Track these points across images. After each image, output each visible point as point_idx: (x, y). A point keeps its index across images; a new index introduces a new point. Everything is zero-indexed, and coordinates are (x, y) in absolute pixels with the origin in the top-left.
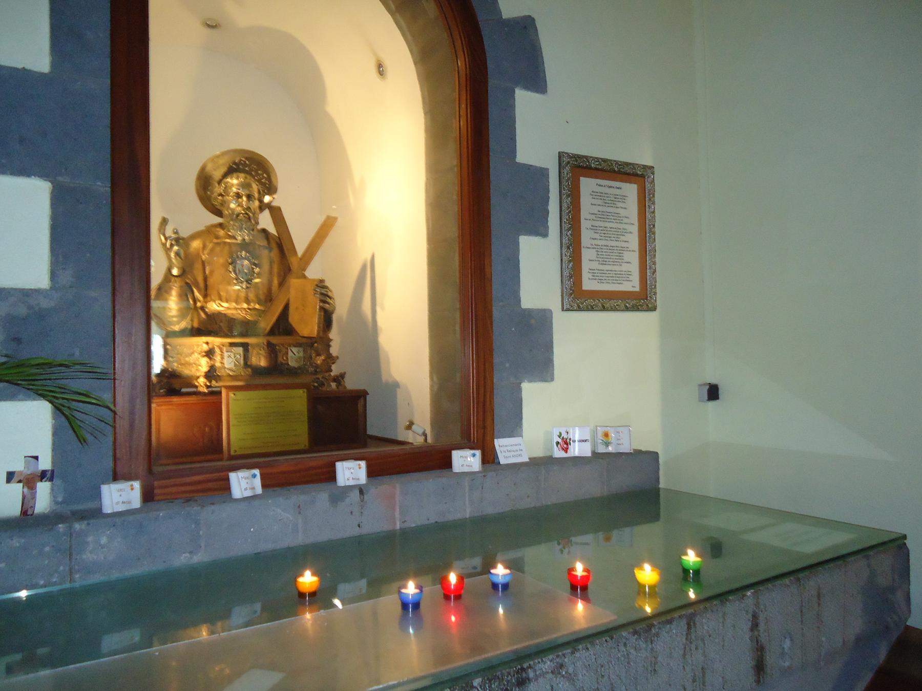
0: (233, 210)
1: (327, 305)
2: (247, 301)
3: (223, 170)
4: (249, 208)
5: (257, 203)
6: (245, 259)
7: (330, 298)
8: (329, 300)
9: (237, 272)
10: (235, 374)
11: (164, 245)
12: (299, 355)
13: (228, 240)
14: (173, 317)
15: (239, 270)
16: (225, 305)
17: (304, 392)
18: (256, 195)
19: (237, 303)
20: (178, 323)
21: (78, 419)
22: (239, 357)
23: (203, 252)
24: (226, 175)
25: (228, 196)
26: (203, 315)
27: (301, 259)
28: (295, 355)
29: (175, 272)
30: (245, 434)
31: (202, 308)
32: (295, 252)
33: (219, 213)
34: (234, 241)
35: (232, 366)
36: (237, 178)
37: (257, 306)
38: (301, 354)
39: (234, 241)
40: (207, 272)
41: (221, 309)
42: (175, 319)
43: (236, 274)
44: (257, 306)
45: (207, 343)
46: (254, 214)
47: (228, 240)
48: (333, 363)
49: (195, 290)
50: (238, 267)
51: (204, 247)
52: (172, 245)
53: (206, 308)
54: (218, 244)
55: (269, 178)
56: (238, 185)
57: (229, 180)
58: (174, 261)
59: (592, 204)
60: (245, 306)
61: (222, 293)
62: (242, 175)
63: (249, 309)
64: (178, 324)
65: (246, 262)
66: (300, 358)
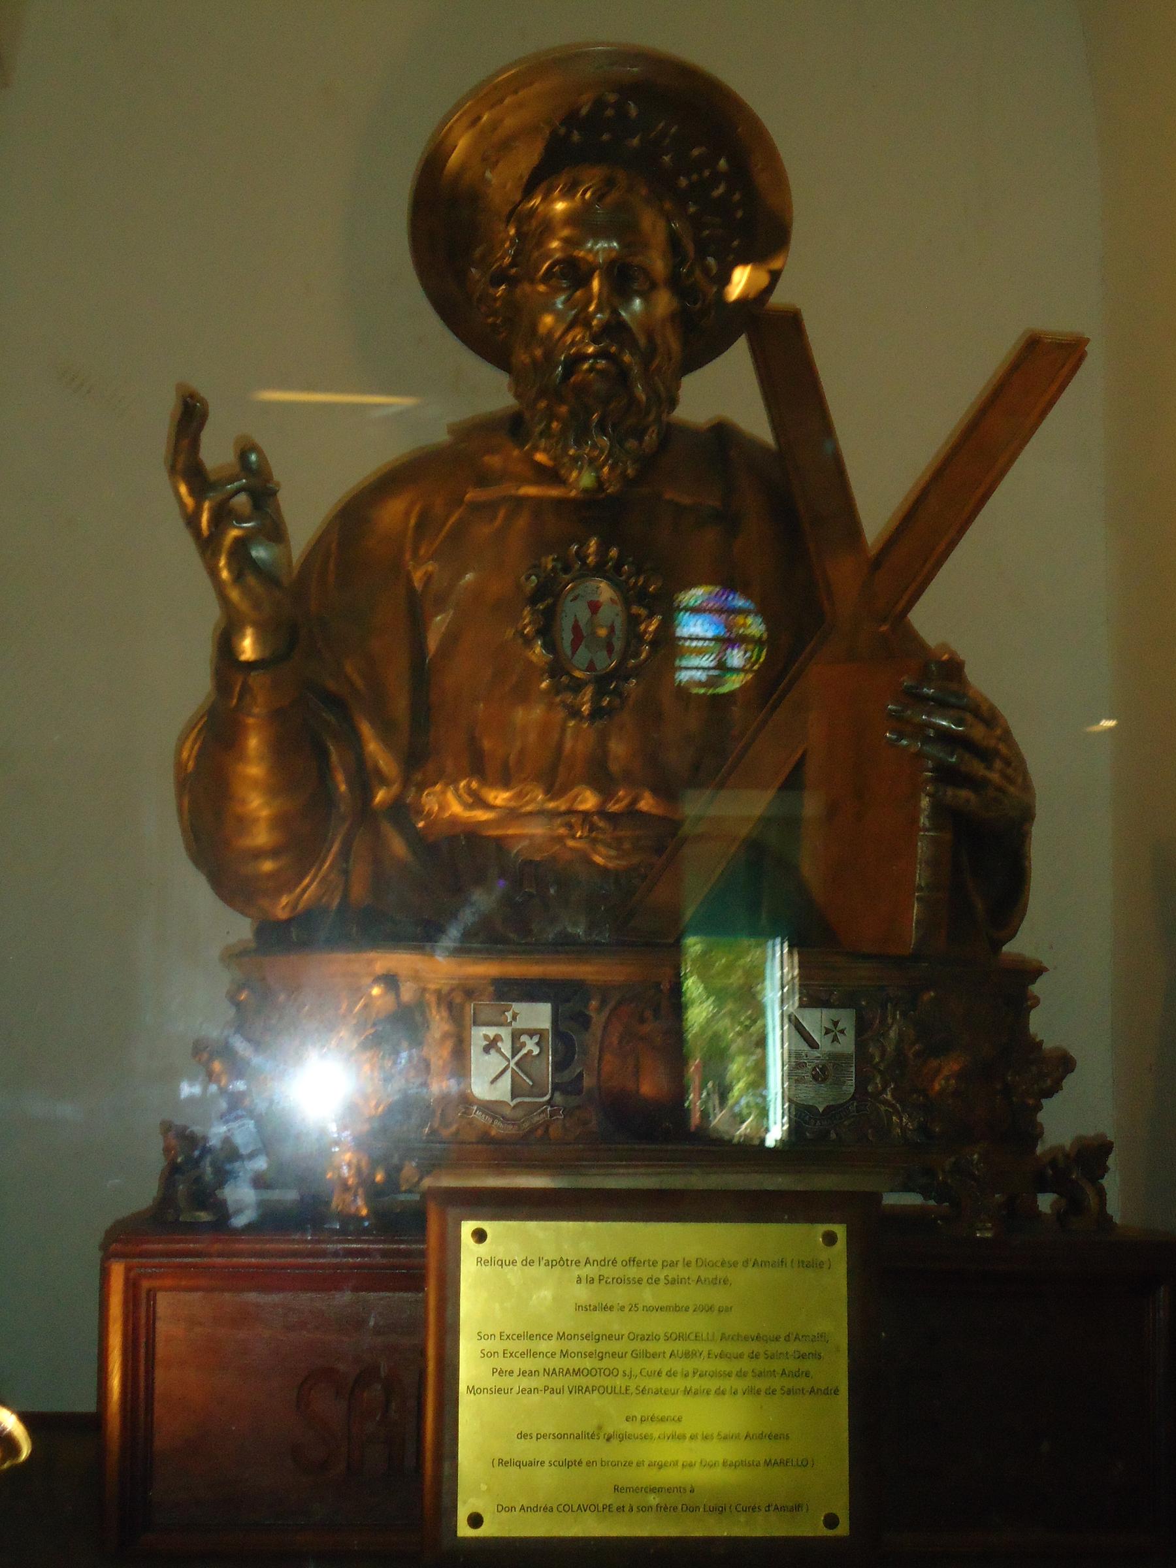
0: (549, 344)
1: (964, 794)
2: (602, 780)
3: (526, 158)
4: (615, 330)
5: (664, 302)
6: (599, 570)
7: (985, 755)
8: (978, 768)
9: (567, 637)
10: (510, 1130)
11: (192, 521)
12: (838, 1048)
13: (531, 490)
14: (258, 854)
15: (576, 628)
16: (500, 797)
17: (830, 1239)
18: (659, 265)
19: (552, 791)
20: (284, 883)
21: (782, 973)
22: (536, 1051)
23: (415, 550)
24: (529, 190)
25: (532, 281)
26: (398, 846)
27: (877, 563)
28: (813, 1044)
29: (248, 647)
30: (522, 1436)
31: (400, 812)
32: (854, 529)
33: (498, 356)
34: (555, 492)
35: (502, 1091)
36: (569, 193)
37: (646, 803)
38: (847, 1044)
39: (555, 492)
40: (433, 643)
41: (482, 815)
42: (268, 866)
43: (550, 646)
44: (646, 803)
45: (390, 981)
46: (647, 357)
47: (531, 490)
48: (1049, 1093)
49: (366, 729)
50: (573, 612)
51: (424, 524)
52: (222, 516)
53: (419, 812)
54: (485, 509)
55: (741, 175)
56: (571, 219)
57: (536, 201)
58: (234, 595)
59: (829, 1268)
60: (589, 801)
61: (487, 744)
62: (591, 178)
63: (612, 818)
64: (288, 887)
65: (605, 591)
66: (836, 1059)
